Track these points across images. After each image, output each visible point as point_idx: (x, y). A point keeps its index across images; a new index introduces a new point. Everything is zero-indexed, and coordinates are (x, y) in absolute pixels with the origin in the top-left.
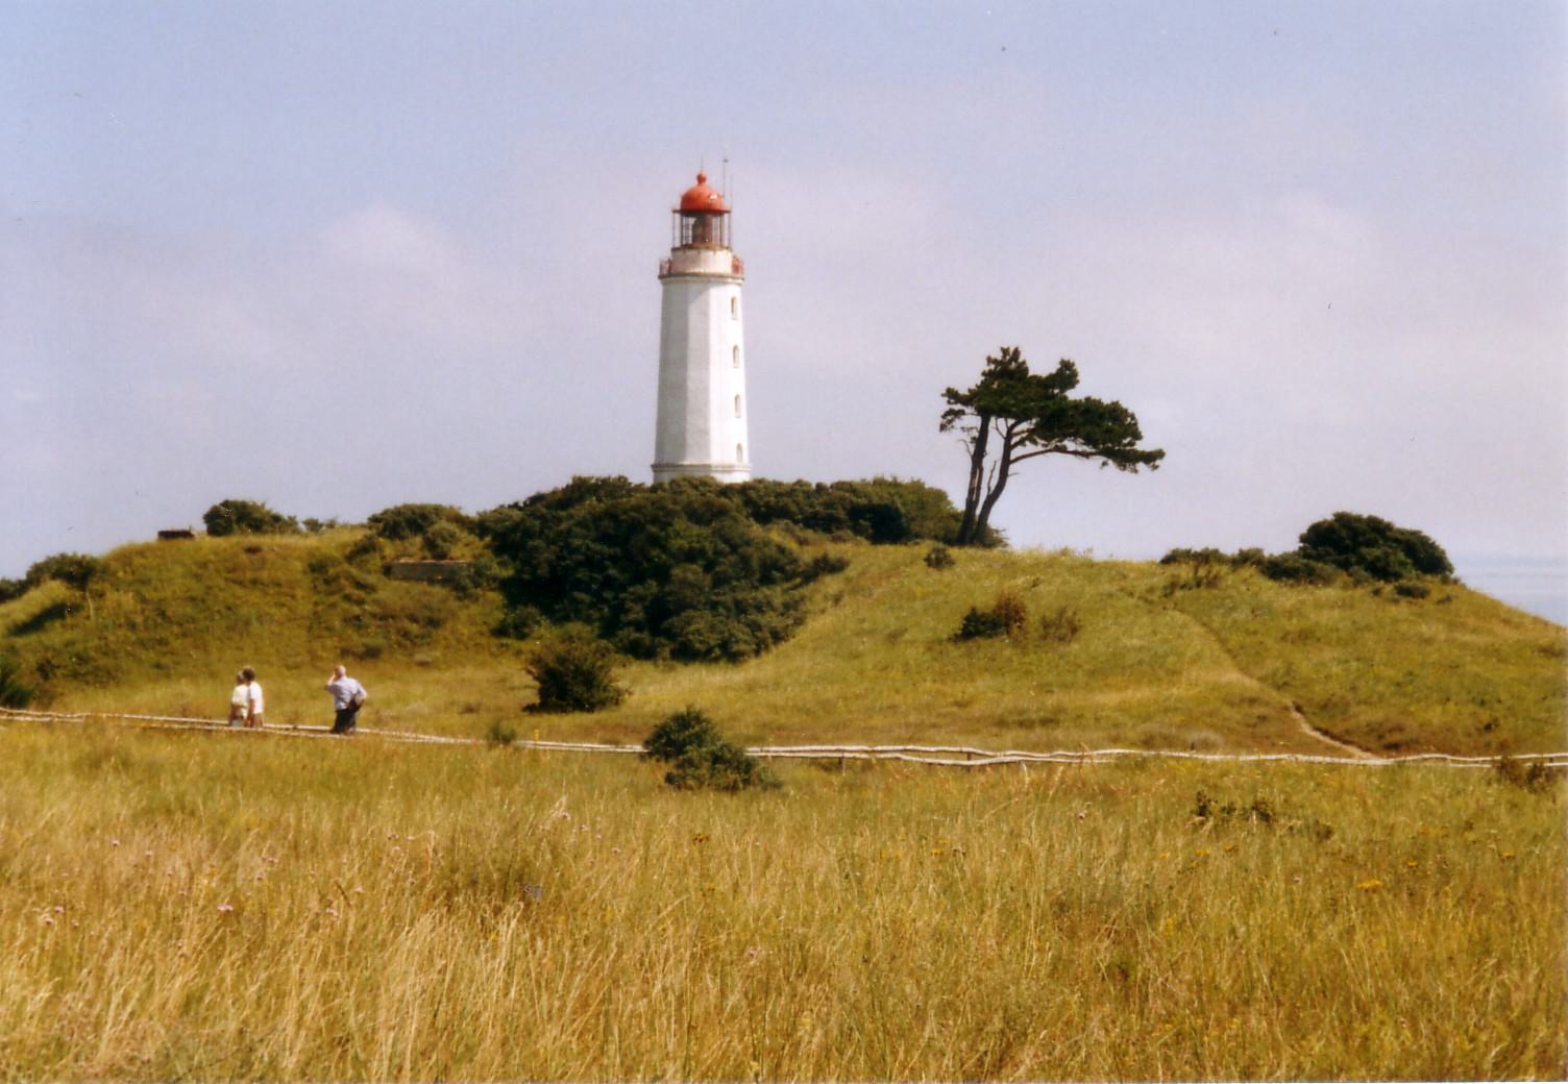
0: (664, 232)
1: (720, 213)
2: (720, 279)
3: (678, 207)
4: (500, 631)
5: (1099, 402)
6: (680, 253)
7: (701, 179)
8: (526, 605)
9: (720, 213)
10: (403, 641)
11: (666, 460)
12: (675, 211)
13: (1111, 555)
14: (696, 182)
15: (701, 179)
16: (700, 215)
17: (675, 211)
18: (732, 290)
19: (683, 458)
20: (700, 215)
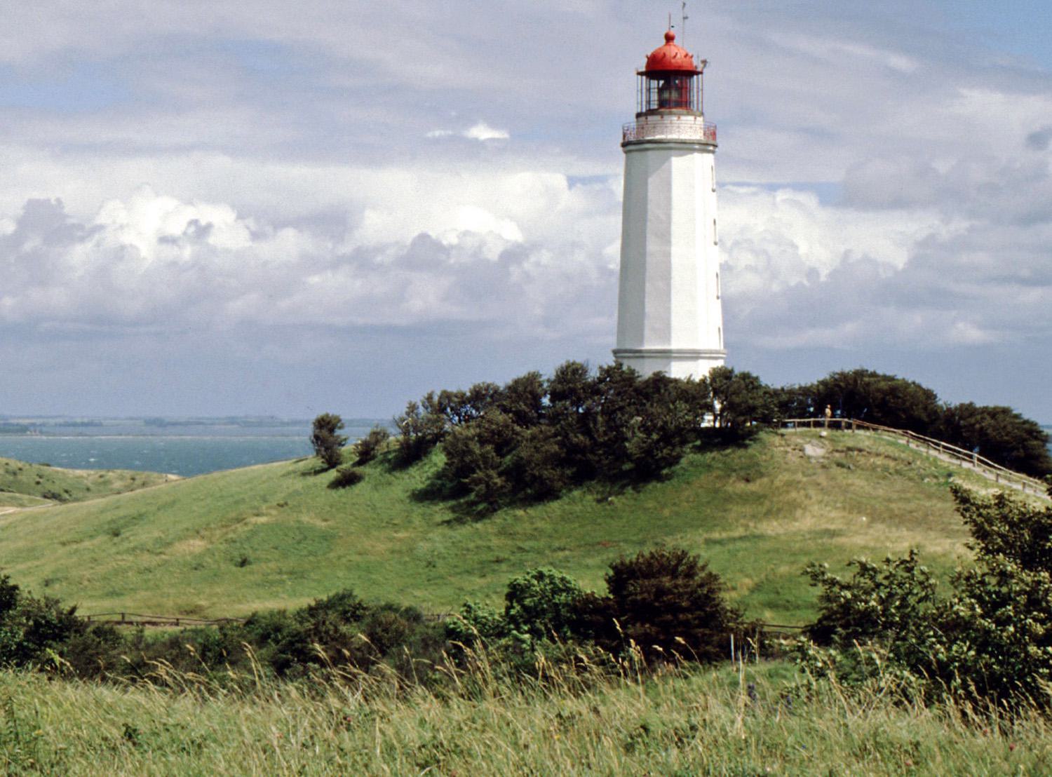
0: (630, 93)
1: (692, 73)
2: (685, 147)
3: (643, 69)
4: (8, 577)
5: (930, 395)
6: (643, 119)
7: (669, 38)
8: (711, 451)
9: (692, 73)
10: (102, 480)
11: (628, 346)
12: (640, 74)
13: (377, 427)
14: (664, 41)
15: (669, 38)
16: (684, 4)
17: (640, 74)
18: (704, 161)
19: (641, 341)
20: (684, 4)
